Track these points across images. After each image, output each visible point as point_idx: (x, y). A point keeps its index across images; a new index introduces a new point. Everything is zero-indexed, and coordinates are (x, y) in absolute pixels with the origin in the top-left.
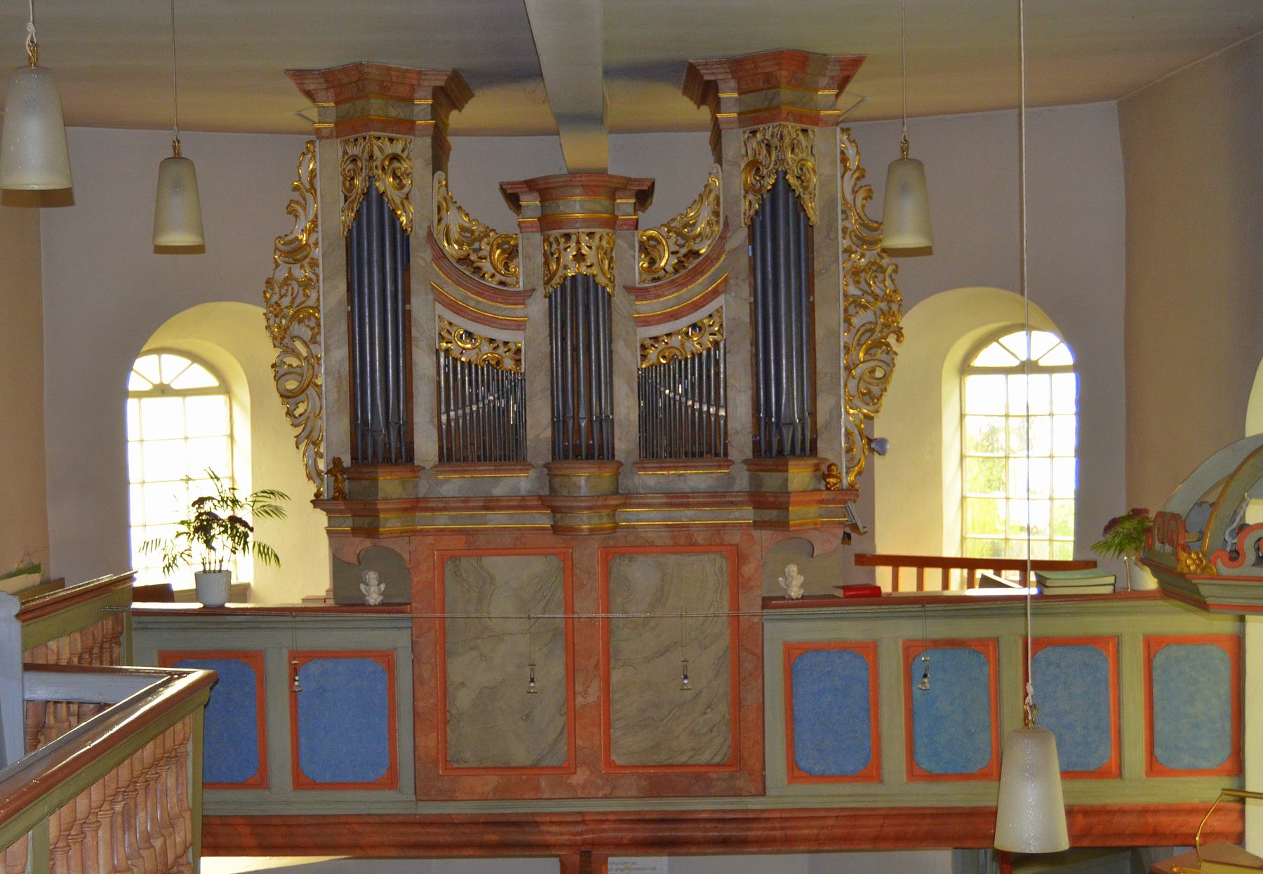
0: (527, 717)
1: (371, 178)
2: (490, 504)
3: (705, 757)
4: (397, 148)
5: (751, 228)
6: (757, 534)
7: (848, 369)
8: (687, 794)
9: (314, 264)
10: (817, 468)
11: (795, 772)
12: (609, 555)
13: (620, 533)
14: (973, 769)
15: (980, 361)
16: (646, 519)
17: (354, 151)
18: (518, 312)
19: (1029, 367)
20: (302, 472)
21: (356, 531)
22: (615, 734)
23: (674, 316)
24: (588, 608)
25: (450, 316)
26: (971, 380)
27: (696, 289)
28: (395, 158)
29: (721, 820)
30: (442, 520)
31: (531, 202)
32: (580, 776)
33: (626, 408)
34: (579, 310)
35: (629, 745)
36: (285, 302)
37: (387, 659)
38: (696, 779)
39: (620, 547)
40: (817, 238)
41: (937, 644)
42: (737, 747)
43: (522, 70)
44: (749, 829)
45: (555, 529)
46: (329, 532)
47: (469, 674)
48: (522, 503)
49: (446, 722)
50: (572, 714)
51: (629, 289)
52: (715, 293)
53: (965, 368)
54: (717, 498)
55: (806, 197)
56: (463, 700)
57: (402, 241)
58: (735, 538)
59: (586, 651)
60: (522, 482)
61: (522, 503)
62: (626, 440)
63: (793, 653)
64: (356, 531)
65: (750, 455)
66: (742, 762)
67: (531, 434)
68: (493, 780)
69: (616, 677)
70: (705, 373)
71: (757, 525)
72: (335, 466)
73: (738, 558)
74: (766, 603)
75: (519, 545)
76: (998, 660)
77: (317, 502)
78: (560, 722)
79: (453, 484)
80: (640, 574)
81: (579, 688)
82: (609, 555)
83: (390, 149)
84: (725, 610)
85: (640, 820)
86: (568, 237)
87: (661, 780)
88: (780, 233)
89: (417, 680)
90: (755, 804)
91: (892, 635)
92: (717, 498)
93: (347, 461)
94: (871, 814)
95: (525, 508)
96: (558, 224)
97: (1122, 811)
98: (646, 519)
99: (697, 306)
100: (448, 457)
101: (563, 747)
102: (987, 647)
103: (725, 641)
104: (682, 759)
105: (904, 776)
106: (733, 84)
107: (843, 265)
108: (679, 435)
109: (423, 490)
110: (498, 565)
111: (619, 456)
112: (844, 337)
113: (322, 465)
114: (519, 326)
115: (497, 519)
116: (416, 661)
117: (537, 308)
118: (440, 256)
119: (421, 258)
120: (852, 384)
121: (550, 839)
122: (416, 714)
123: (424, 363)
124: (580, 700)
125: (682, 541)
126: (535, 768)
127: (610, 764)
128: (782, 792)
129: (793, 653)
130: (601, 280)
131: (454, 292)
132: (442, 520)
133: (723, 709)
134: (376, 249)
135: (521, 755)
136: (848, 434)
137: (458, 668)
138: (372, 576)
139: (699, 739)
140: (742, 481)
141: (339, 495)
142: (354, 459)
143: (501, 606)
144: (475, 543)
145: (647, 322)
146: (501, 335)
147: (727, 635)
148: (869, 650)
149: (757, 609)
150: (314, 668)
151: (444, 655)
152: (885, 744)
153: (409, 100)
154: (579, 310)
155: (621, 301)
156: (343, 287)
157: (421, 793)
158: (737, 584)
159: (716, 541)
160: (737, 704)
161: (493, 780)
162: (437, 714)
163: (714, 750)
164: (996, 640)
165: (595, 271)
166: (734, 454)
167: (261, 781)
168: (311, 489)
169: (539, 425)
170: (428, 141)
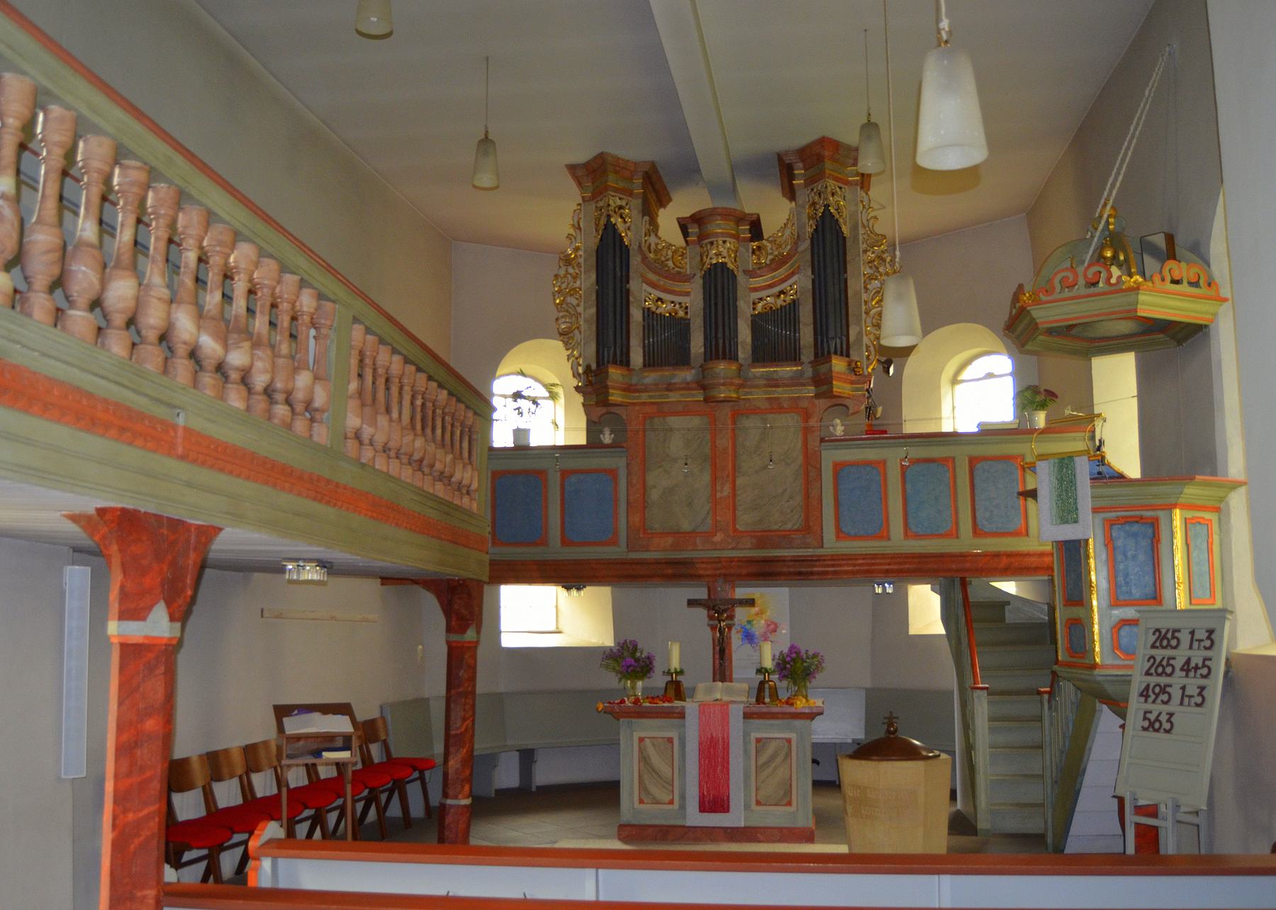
0: (690, 504)
1: (609, 216)
2: (670, 388)
3: (789, 526)
4: (623, 203)
5: (812, 240)
6: (817, 402)
7: (867, 313)
8: (779, 547)
9: (579, 265)
10: (849, 364)
11: (840, 534)
12: (735, 416)
13: (742, 403)
14: (942, 531)
15: (965, 375)
16: (758, 396)
17: (601, 204)
18: (686, 287)
19: (990, 376)
20: (570, 373)
21: (597, 404)
22: (739, 513)
23: (770, 286)
24: (724, 442)
25: (650, 289)
26: (958, 387)
27: (782, 272)
28: (621, 207)
29: (797, 560)
30: (644, 397)
31: (693, 230)
32: (718, 537)
33: (744, 333)
34: (719, 285)
35: (746, 520)
36: (564, 286)
37: (613, 473)
38: (783, 538)
39: (740, 411)
40: (848, 244)
41: (919, 461)
42: (807, 519)
43: (690, 171)
44: (773, 278)
45: (706, 400)
46: (584, 405)
47: (658, 481)
48: (686, 387)
49: (645, 508)
50: (714, 501)
51: (745, 272)
52: (793, 274)
53: (955, 381)
54: (796, 381)
55: (841, 220)
56: (654, 495)
57: (624, 251)
58: (805, 404)
59: (722, 465)
60: (687, 375)
61: (686, 387)
62: (744, 352)
63: (838, 468)
64: (597, 404)
65: (812, 358)
66: (810, 526)
67: (693, 350)
68: (670, 540)
69: (739, 481)
70: (788, 314)
71: (817, 396)
72: (588, 369)
73: (807, 415)
74: (822, 440)
75: (686, 411)
76: (954, 468)
77: (577, 388)
78: (707, 507)
79: (651, 377)
80: (751, 424)
81: (718, 488)
82: (735, 416)
83: (619, 202)
84: (800, 445)
85: (751, 561)
86: (712, 243)
87: (764, 539)
88: (828, 246)
89: (629, 484)
90: (820, 552)
91: (894, 457)
92: (796, 381)
93: (594, 366)
94: (884, 556)
95: (690, 389)
96: (707, 236)
97: (1028, 555)
98: (758, 396)
99: (783, 281)
100: (649, 363)
101: (709, 521)
102: (948, 462)
103: (800, 460)
104: (776, 527)
105: (902, 536)
106: (801, 165)
107: (863, 258)
108: (774, 340)
109: (634, 380)
110: (674, 421)
111: (741, 361)
112: (864, 297)
113: (581, 370)
114: (687, 294)
115: (674, 397)
116: (629, 474)
117: (698, 283)
118: (644, 258)
119: (635, 260)
120: (869, 320)
121: (701, 572)
122: (628, 503)
123: (636, 315)
124: (719, 495)
125: (776, 407)
126: (693, 533)
127: (735, 530)
128: (832, 544)
129: (838, 468)
130: (730, 266)
131: (651, 276)
132: (644, 397)
133: (799, 499)
134: (612, 258)
135: (686, 526)
136: (868, 347)
137: (651, 478)
138: (607, 432)
139: (785, 516)
140: (809, 372)
141: (590, 383)
142: (598, 363)
143: (676, 446)
144: (663, 411)
145: (755, 290)
146: (677, 299)
147: (801, 458)
148: (882, 464)
149: (817, 443)
150: (573, 479)
151: (644, 471)
152: (891, 517)
153: (630, 179)
154: (719, 285)
155: (741, 278)
156: (594, 276)
157: (630, 548)
158: (806, 431)
159: (795, 406)
160: (807, 496)
161: (670, 540)
162: (640, 504)
163: (795, 521)
164: (953, 459)
165: (726, 260)
166: (803, 358)
167: (543, 542)
168: (575, 382)
169: (697, 344)
170: (640, 201)
